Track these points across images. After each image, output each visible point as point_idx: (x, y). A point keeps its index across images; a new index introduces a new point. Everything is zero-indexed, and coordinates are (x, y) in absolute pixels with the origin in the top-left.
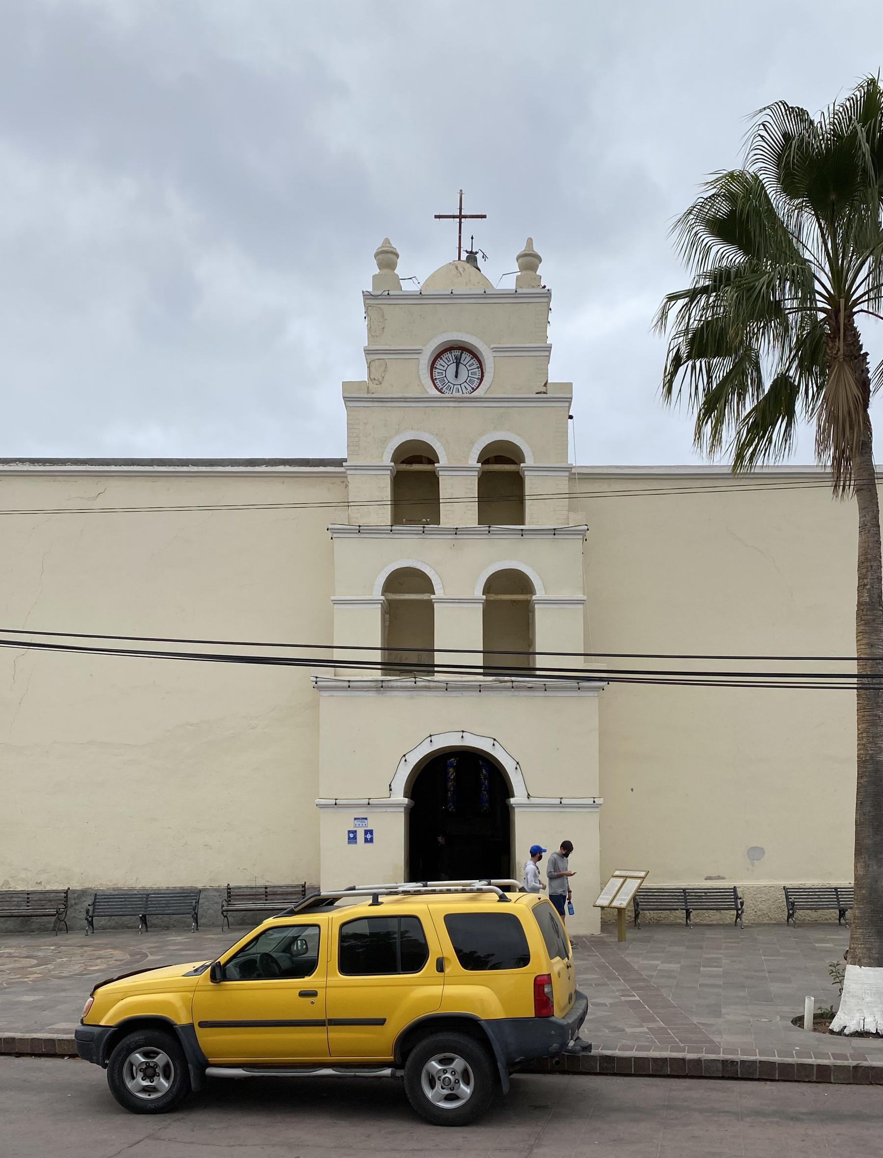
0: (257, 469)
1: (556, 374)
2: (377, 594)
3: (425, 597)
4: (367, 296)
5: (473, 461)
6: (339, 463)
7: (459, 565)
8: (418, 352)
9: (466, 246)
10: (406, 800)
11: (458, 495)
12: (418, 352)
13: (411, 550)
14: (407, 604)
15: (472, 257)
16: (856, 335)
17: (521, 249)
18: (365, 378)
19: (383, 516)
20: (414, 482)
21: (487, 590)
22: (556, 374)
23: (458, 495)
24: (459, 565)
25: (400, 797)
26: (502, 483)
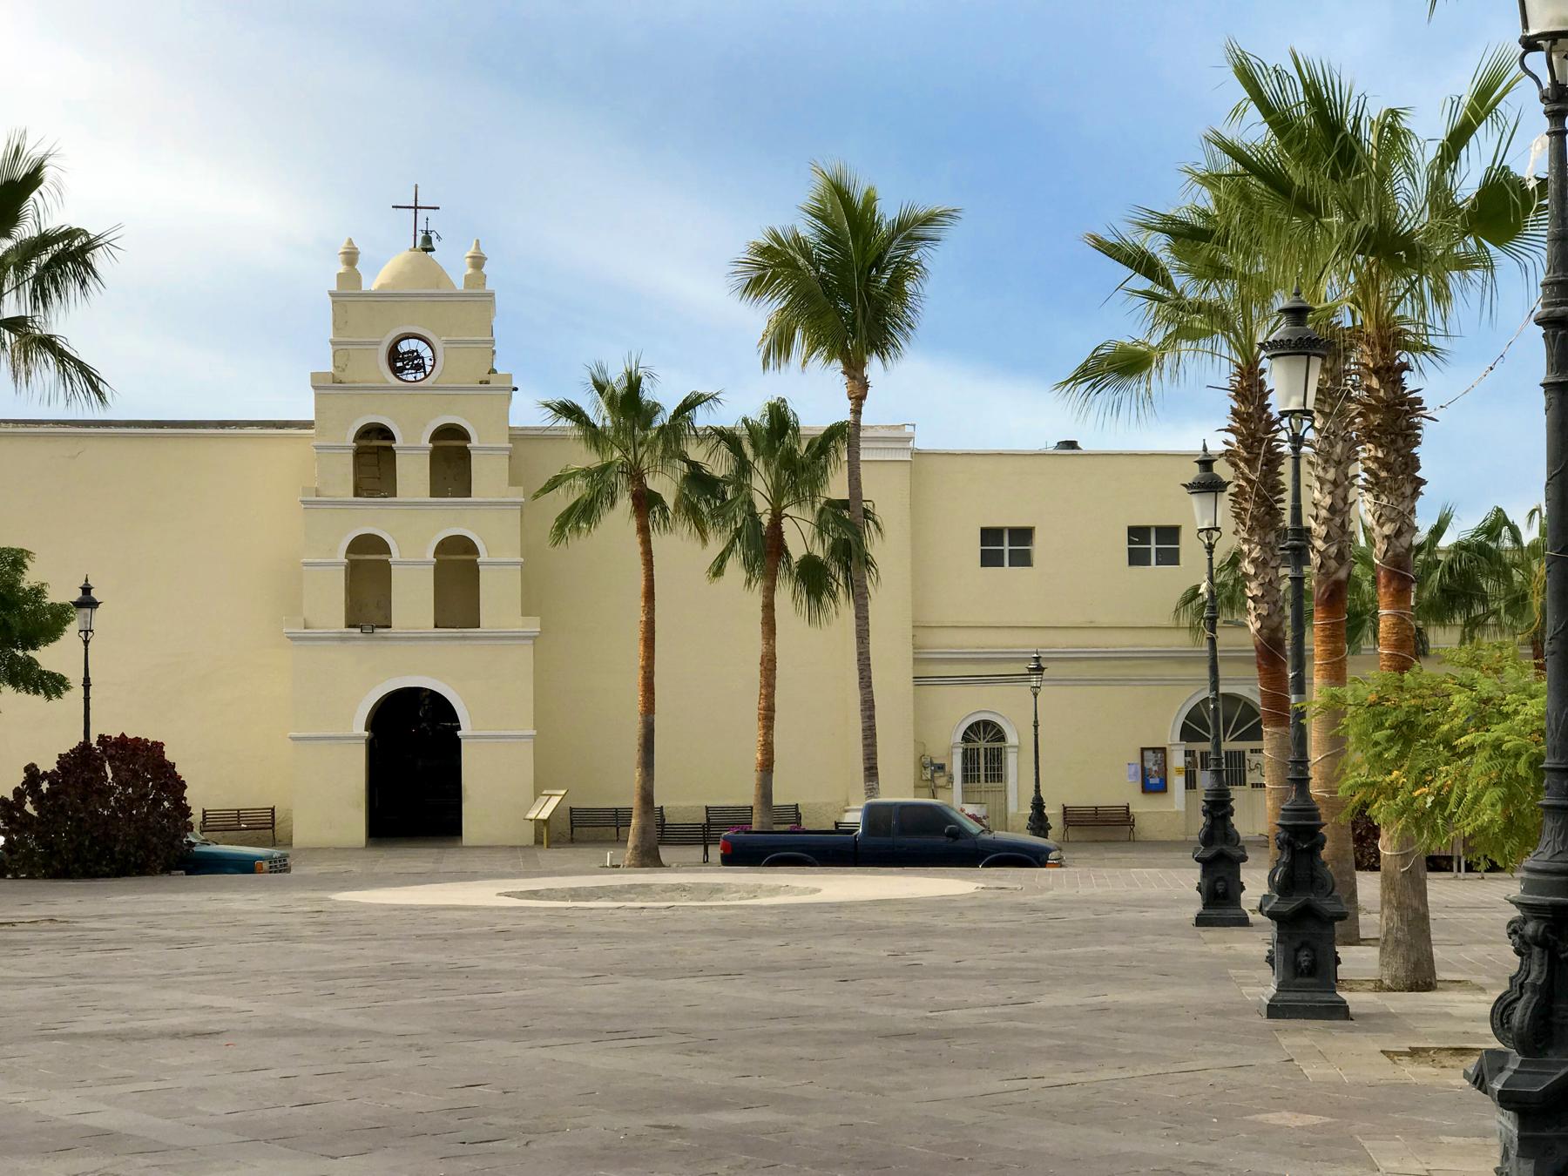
0: (227, 431)
1: (489, 287)
2: (341, 557)
3: (384, 557)
4: (332, 294)
5: (425, 442)
6: (307, 425)
7: (413, 527)
8: (378, 343)
9: (421, 226)
10: (367, 734)
11: (413, 470)
12: (378, 343)
13: (372, 518)
14: (368, 567)
15: (427, 239)
16: (781, 534)
17: (471, 252)
18: (330, 369)
19: (346, 489)
20: (374, 454)
21: (436, 553)
22: (489, 287)
23: (413, 470)
24: (413, 527)
25: (359, 729)
26: (451, 457)
